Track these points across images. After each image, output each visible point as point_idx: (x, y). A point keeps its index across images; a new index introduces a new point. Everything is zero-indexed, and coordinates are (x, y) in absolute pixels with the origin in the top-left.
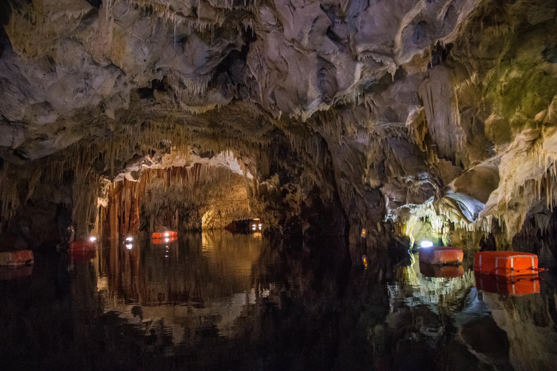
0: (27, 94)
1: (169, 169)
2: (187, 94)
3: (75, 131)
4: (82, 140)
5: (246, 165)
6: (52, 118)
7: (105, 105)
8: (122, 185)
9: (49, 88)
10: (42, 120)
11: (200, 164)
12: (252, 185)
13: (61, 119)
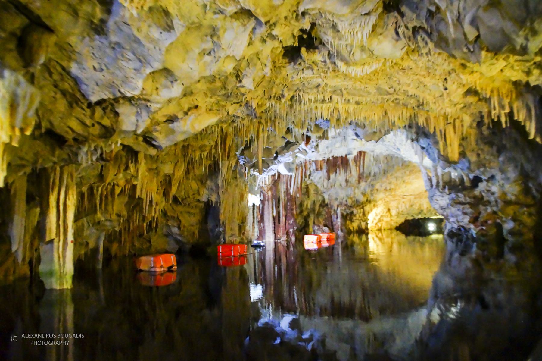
0: (142, 59)
1: (328, 160)
2: (344, 47)
3: (210, 110)
4: (221, 121)
5: (423, 148)
6: (176, 90)
7: (242, 73)
8: (277, 179)
9: (168, 50)
10: (165, 94)
11: (364, 153)
12: (432, 175)
13: (187, 93)
